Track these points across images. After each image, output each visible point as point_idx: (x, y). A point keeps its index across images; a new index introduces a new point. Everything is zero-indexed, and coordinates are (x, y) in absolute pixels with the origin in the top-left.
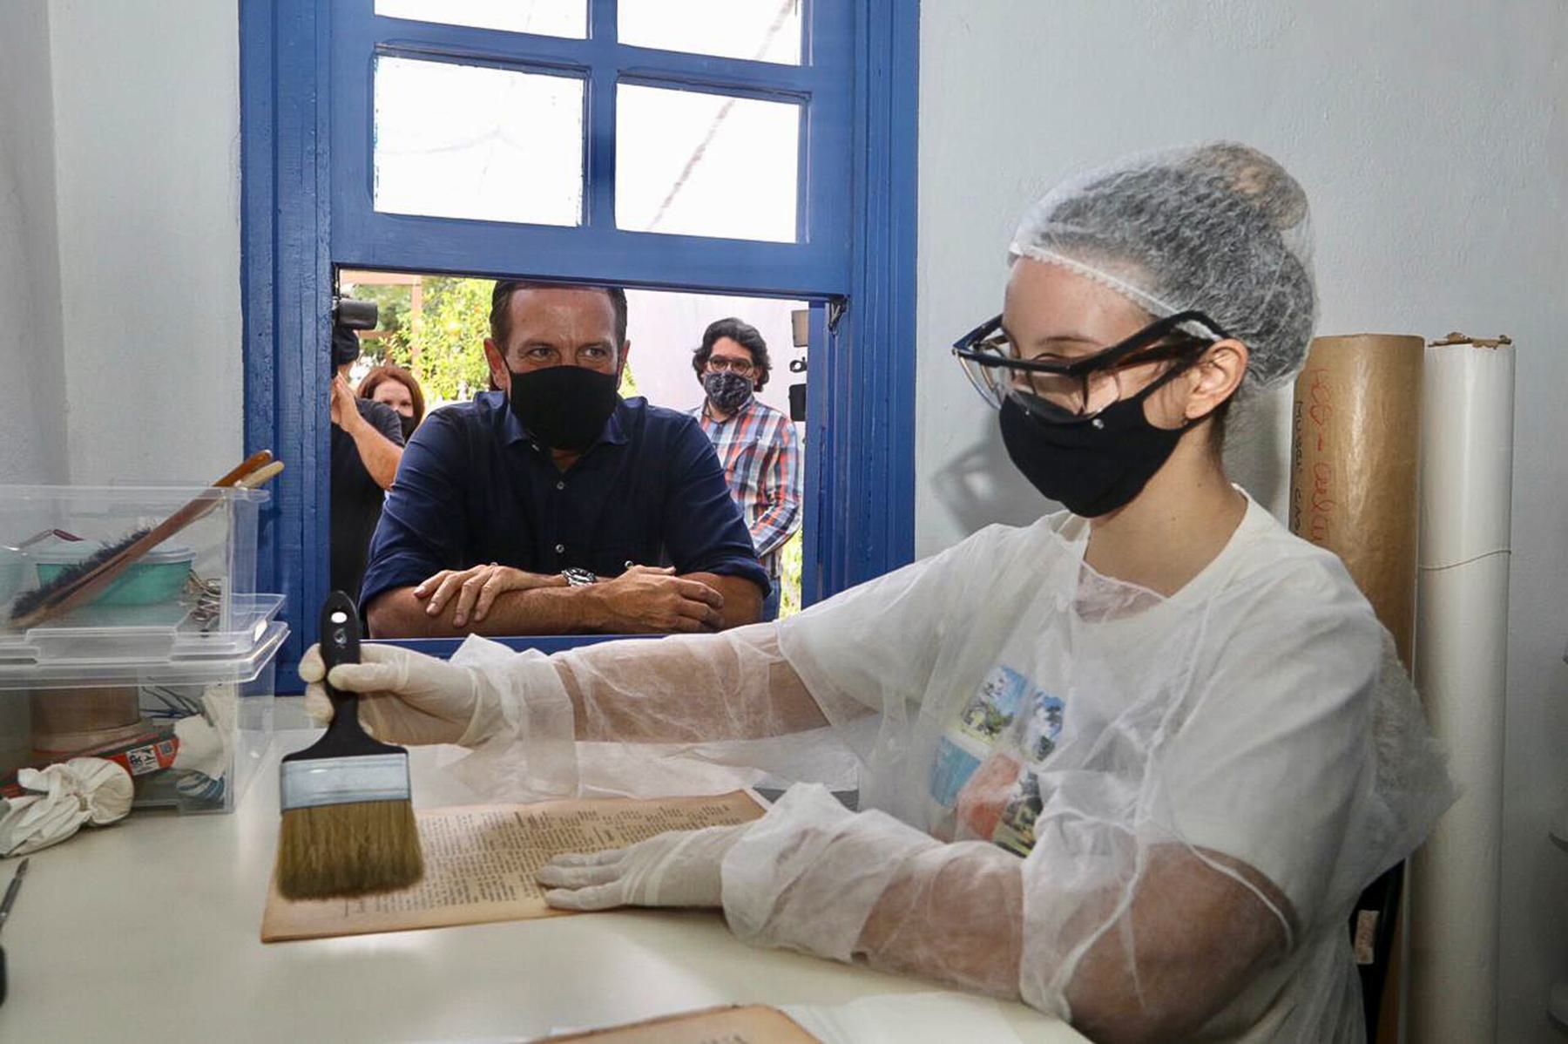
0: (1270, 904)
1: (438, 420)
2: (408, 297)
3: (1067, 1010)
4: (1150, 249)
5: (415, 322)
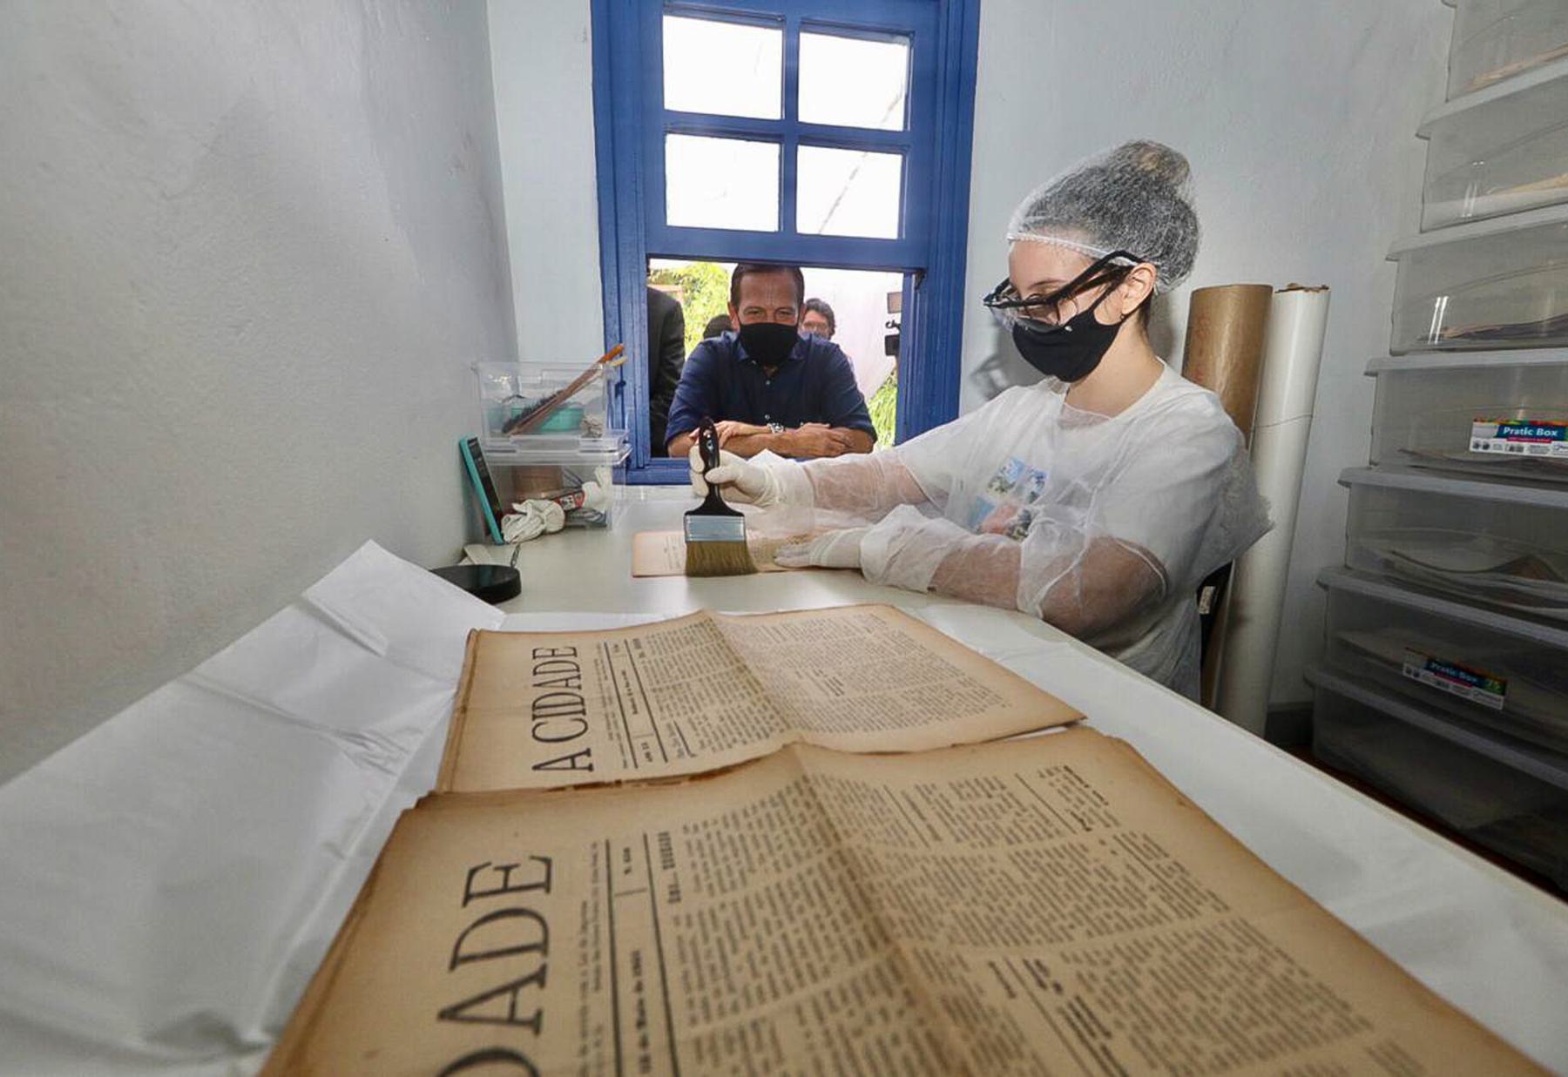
3: (1041, 615)
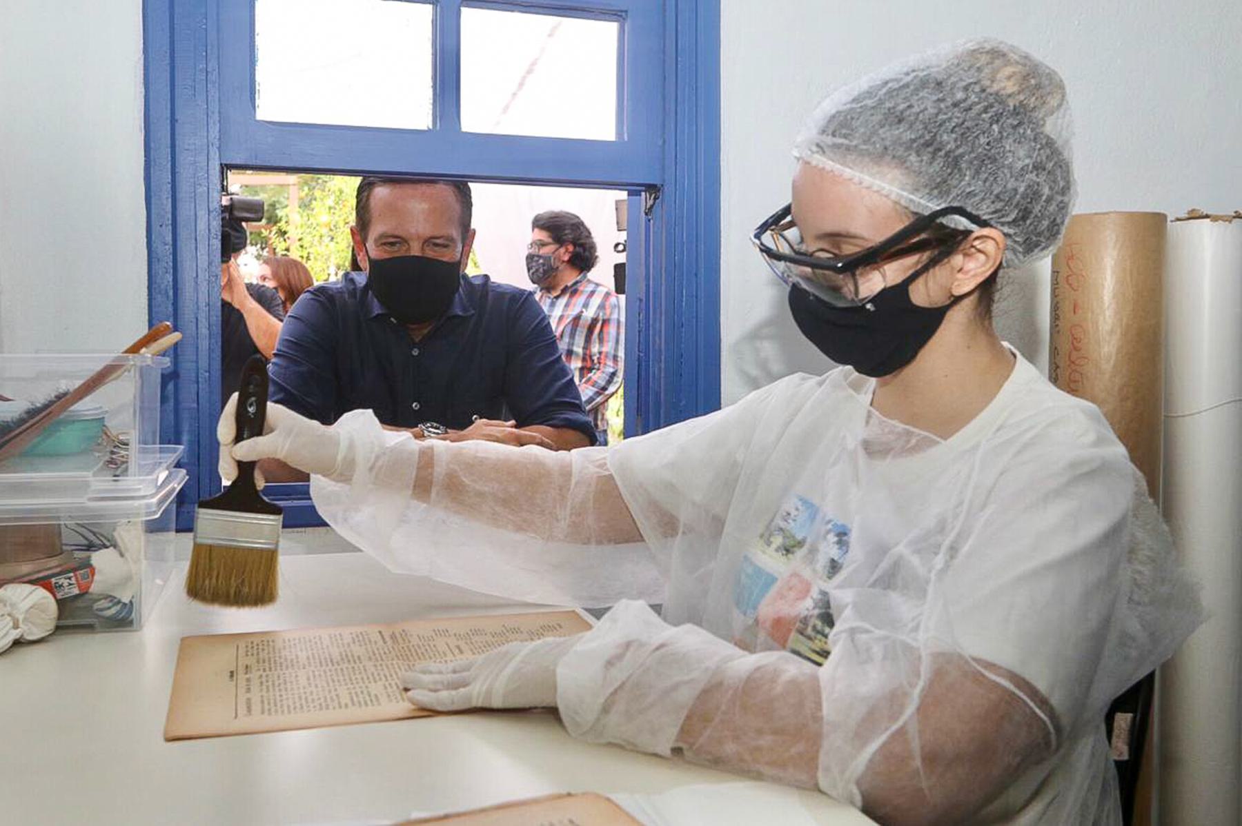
0: (1037, 711)
1: (312, 296)
2: (286, 195)
3: (858, 799)
4: (910, 155)
5: (291, 215)
